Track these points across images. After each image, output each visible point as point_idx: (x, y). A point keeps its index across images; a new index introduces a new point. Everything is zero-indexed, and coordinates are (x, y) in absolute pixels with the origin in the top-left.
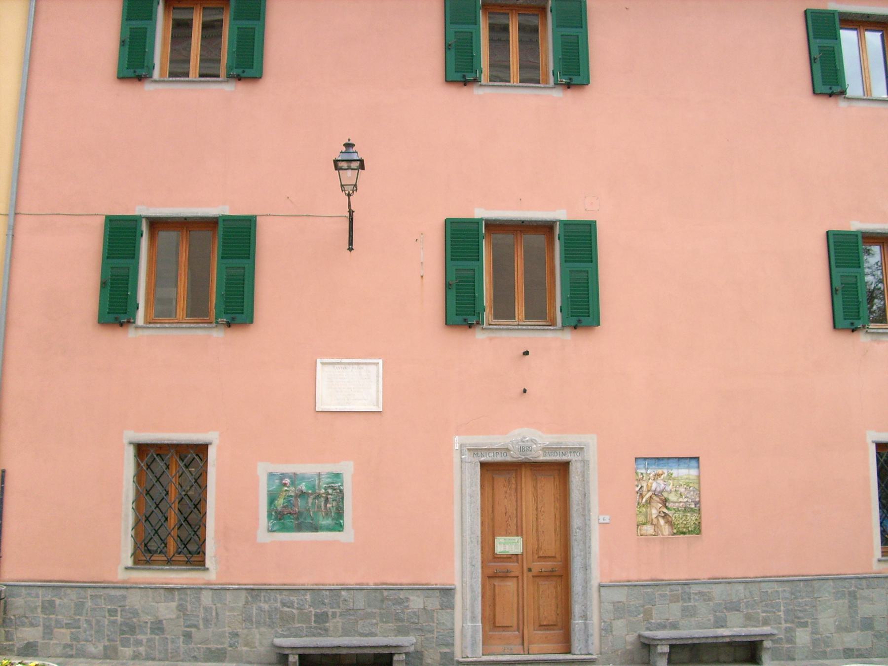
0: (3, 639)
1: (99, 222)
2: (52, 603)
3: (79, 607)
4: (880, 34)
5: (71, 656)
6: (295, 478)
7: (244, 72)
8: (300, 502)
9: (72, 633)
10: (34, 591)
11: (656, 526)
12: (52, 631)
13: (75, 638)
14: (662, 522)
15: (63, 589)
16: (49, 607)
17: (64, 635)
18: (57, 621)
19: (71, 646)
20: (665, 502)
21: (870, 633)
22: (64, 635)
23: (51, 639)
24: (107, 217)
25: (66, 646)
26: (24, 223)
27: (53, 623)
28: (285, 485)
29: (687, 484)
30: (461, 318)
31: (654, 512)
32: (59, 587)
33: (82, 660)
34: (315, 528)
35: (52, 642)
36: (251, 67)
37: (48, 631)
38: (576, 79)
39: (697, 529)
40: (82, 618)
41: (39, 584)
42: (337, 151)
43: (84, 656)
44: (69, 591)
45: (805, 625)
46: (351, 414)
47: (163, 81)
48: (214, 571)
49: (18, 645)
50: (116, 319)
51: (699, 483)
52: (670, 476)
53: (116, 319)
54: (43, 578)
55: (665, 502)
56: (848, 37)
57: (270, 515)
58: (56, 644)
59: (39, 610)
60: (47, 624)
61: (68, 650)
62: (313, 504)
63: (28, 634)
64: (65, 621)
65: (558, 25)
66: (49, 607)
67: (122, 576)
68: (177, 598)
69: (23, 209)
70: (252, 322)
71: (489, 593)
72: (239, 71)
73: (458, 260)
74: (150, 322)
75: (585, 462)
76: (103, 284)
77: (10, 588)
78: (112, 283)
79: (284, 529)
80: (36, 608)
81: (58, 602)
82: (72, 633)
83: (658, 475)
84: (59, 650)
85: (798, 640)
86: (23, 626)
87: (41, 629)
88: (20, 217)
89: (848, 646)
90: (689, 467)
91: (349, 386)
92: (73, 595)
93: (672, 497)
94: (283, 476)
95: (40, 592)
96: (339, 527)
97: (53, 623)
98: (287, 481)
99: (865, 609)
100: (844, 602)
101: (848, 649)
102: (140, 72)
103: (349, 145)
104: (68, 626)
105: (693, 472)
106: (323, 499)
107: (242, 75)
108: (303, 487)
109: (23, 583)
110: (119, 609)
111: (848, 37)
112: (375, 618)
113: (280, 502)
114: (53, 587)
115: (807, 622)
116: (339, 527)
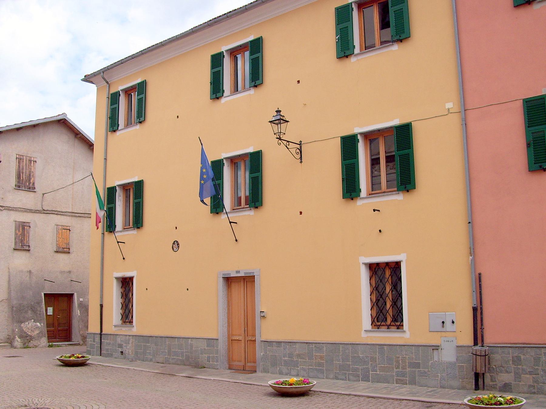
0: (489, 381)
1: (520, 104)
2: (519, 358)
3: (537, 360)
5: (534, 393)
7: (400, 36)
9: (533, 378)
10: (506, 350)
12: (520, 376)
13: (536, 381)
15: (525, 349)
16: (517, 360)
17: (528, 379)
18: (523, 369)
19: (533, 386)
22: (528, 379)
23: (520, 381)
24: (523, 100)
25: (530, 386)
26: (471, 115)
27: (521, 371)
30: (538, 165)
32: (523, 347)
33: (542, 396)
35: (521, 383)
36: (348, 49)
37: (518, 376)
40: (540, 368)
41: (509, 345)
42: (272, 115)
43: (543, 393)
44: (529, 350)
47: (363, 53)
49: (499, 385)
50: (541, 166)
53: (541, 166)
54: (512, 342)
58: (523, 385)
59: (511, 362)
60: (517, 371)
61: (532, 389)
63: (504, 378)
64: (528, 370)
66: (517, 360)
69: (468, 107)
70: (415, 188)
72: (398, 37)
73: (533, 126)
74: (370, 195)
76: (528, 145)
77: (491, 348)
78: (534, 143)
80: (508, 361)
81: (522, 357)
82: (533, 378)
84: (526, 389)
86: (501, 372)
87: (513, 374)
88: (467, 112)
92: (532, 352)
95: (510, 350)
97: (521, 371)
102: (348, 53)
103: (278, 111)
104: (530, 373)
107: (401, 38)
109: (499, 345)
112: (285, 361)
114: (519, 347)
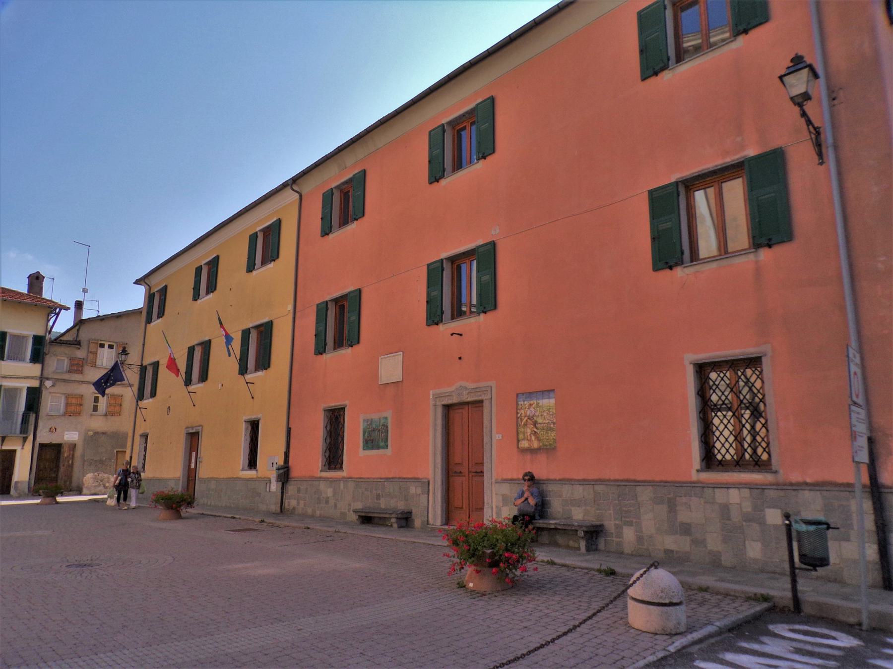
4: (741, 179)
11: (530, 440)
14: (533, 438)
20: (535, 424)
21: (688, 538)
29: (549, 410)
31: (529, 431)
34: (378, 448)
39: (554, 449)
45: (630, 524)
46: (123, 321)
55: (535, 424)
67: (695, 476)
71: (191, 483)
83: (530, 405)
85: (625, 536)
89: (668, 547)
90: (549, 398)
93: (540, 420)
99: (684, 516)
100: (663, 509)
101: (668, 550)
105: (553, 401)
115: (632, 522)
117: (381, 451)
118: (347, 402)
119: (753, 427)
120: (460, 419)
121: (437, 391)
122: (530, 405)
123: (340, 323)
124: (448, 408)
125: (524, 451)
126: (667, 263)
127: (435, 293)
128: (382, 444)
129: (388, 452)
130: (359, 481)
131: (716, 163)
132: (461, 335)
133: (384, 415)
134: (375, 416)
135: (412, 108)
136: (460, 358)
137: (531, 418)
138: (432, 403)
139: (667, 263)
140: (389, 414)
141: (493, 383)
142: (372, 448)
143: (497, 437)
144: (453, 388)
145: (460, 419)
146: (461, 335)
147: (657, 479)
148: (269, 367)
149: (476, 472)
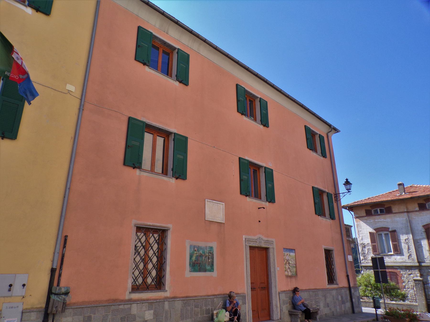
6: (199, 248)
8: (200, 259)
20: (289, 263)
28: (195, 250)
34: (205, 271)
38: (266, 125)
48: (168, 291)
51: (296, 267)
52: (290, 255)
56: (148, 137)
57: (190, 264)
62: (205, 259)
65: (392, 242)
68: (154, 307)
75: (273, 248)
79: (195, 271)
91: (215, 211)
93: (290, 262)
94: (194, 247)
96: (212, 270)
98: (196, 249)
106: (207, 258)
108: (201, 252)
110: (126, 317)
111: (148, 137)
113: (194, 258)
116: (212, 270)
117: (208, 274)
118: (170, 226)
119: (145, 278)
120: (260, 256)
121: (248, 237)
122: (287, 254)
123: (254, 180)
124: (266, 249)
125: (287, 276)
126: (134, 164)
127: (270, 185)
128: (208, 268)
129: (215, 274)
130: (186, 300)
131: (160, 125)
132: (259, 208)
133: (210, 244)
134: (202, 244)
135: (269, 86)
136: (259, 221)
137: (288, 260)
138: (244, 245)
139: (134, 164)
140: (214, 245)
141: (274, 240)
142: (200, 271)
143: (278, 269)
144: (256, 238)
145: (260, 256)
146: (259, 208)
147: (307, 289)
148: (186, 179)
149: (262, 288)
